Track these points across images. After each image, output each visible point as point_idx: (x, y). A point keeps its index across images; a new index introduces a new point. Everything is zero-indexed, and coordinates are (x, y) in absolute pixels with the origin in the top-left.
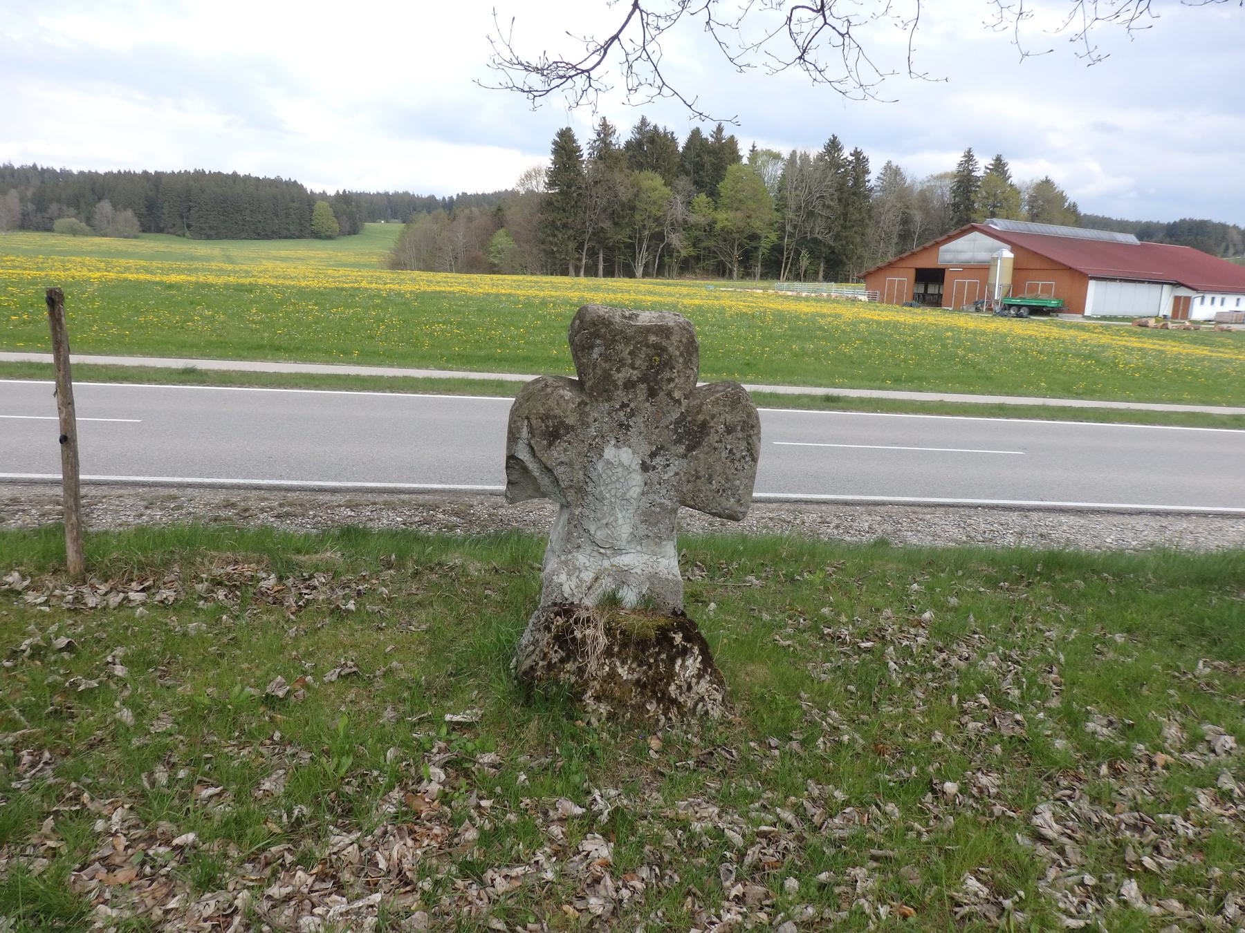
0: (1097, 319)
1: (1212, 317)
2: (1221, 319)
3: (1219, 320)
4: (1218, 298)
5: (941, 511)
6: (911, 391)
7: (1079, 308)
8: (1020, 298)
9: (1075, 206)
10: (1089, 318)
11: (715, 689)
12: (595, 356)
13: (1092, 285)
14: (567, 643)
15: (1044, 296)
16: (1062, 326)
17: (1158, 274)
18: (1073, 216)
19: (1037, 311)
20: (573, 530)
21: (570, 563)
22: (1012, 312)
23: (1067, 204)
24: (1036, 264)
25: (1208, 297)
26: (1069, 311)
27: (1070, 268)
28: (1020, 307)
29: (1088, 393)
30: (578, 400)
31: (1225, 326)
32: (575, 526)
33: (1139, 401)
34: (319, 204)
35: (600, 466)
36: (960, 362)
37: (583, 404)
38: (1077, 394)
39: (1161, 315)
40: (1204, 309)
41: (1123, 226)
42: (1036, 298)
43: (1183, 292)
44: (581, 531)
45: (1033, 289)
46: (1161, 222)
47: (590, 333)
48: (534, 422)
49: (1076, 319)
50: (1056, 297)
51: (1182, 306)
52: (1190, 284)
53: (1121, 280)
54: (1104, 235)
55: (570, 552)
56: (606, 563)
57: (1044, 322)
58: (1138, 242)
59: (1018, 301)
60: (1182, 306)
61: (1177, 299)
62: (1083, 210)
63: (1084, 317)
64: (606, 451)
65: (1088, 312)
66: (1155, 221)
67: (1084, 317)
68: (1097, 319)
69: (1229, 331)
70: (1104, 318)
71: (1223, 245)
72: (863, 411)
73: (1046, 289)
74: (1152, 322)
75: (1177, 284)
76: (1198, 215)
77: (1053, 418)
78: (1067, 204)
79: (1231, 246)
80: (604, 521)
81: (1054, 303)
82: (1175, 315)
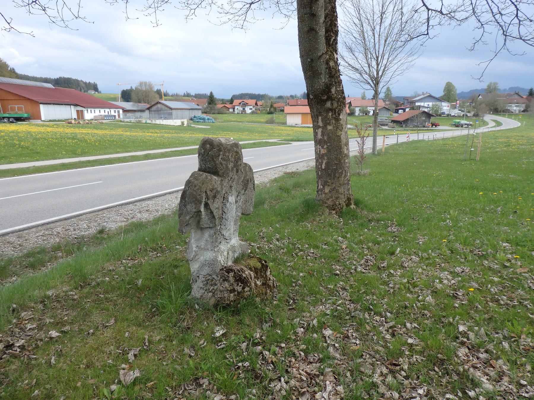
0: (48, 121)
1: (93, 118)
2: (96, 119)
3: (95, 119)
4: (93, 110)
5: (105, 211)
6: (7, 164)
7: (39, 117)
8: (8, 114)
9: (13, 69)
10: (44, 121)
11: (251, 279)
12: (220, 159)
13: (42, 107)
14: (241, 280)
15: (19, 112)
16: (30, 125)
17: (68, 101)
18: (13, 73)
19: (19, 119)
20: (218, 236)
21: (220, 251)
22: (6, 121)
23: (9, 68)
24: (12, 97)
25: (89, 110)
26: (34, 119)
27: (29, 99)
28: (9, 118)
29: (83, 154)
30: (220, 179)
31: (101, 121)
32: (219, 234)
33: (105, 154)
34: (53, 84)
35: (228, 205)
36: (19, 147)
37: (222, 180)
38: (79, 155)
39: (73, 118)
40: (89, 115)
41: (46, 80)
42: (16, 113)
43: (79, 108)
44: (221, 236)
45: (13, 109)
46: (51, 78)
47: (218, 150)
48: (208, 193)
49: (38, 122)
50: (26, 113)
51: (80, 114)
52: (81, 105)
53: (53, 104)
54: (38, 84)
55: (218, 246)
56: (229, 246)
57: (27, 124)
58: (54, 87)
59: (7, 115)
60: (80, 114)
61: (78, 111)
62: (19, 71)
63: (42, 121)
64: (229, 198)
65: (43, 119)
66: (49, 77)
67: (42, 121)
68: (48, 121)
69: (103, 123)
70: (50, 121)
71: (79, 88)
72: (8, 177)
73: (20, 109)
74: (73, 121)
75: (76, 105)
76: (66, 75)
77: (93, 166)
78: (9, 68)
79: (82, 89)
80: (228, 229)
81: (26, 115)
82: (78, 118)
